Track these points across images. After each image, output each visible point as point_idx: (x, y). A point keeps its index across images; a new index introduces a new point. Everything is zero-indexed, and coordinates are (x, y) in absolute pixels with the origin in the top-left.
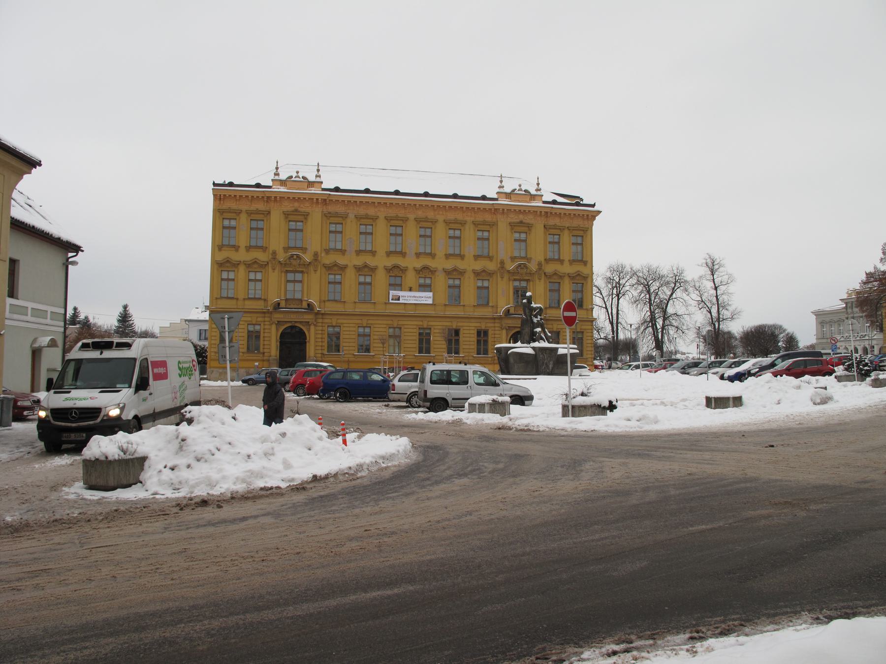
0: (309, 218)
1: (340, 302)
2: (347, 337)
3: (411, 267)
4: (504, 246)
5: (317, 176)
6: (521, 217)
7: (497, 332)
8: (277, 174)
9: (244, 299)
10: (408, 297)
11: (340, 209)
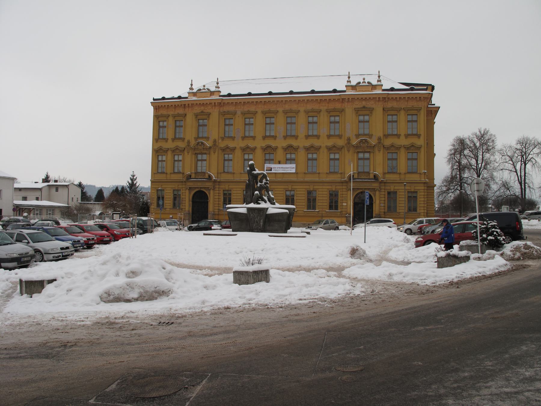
0: (211, 116)
1: (396, 173)
2: (235, 197)
3: (259, 146)
4: (350, 126)
5: (378, 81)
6: (364, 103)
7: (344, 193)
8: (191, 89)
9: (405, 174)
10: (278, 168)
11: (232, 109)
